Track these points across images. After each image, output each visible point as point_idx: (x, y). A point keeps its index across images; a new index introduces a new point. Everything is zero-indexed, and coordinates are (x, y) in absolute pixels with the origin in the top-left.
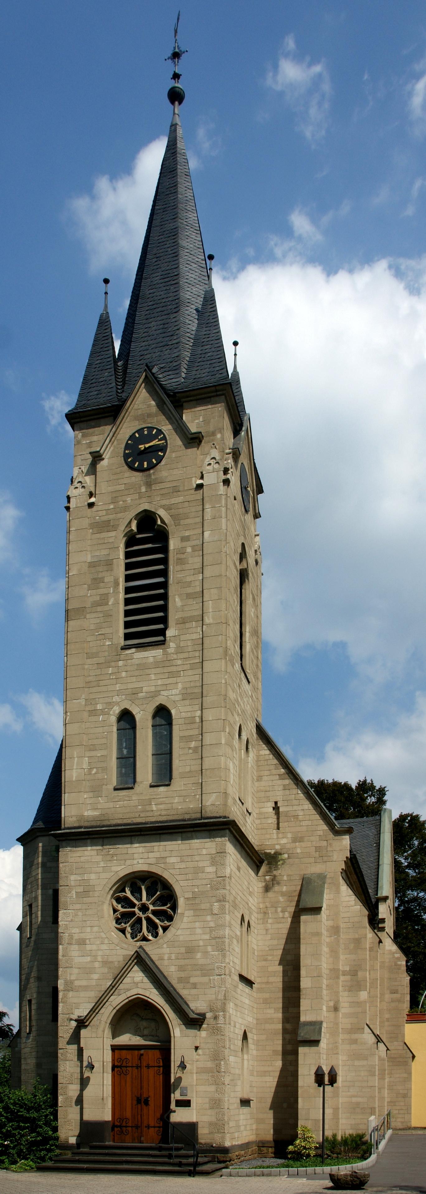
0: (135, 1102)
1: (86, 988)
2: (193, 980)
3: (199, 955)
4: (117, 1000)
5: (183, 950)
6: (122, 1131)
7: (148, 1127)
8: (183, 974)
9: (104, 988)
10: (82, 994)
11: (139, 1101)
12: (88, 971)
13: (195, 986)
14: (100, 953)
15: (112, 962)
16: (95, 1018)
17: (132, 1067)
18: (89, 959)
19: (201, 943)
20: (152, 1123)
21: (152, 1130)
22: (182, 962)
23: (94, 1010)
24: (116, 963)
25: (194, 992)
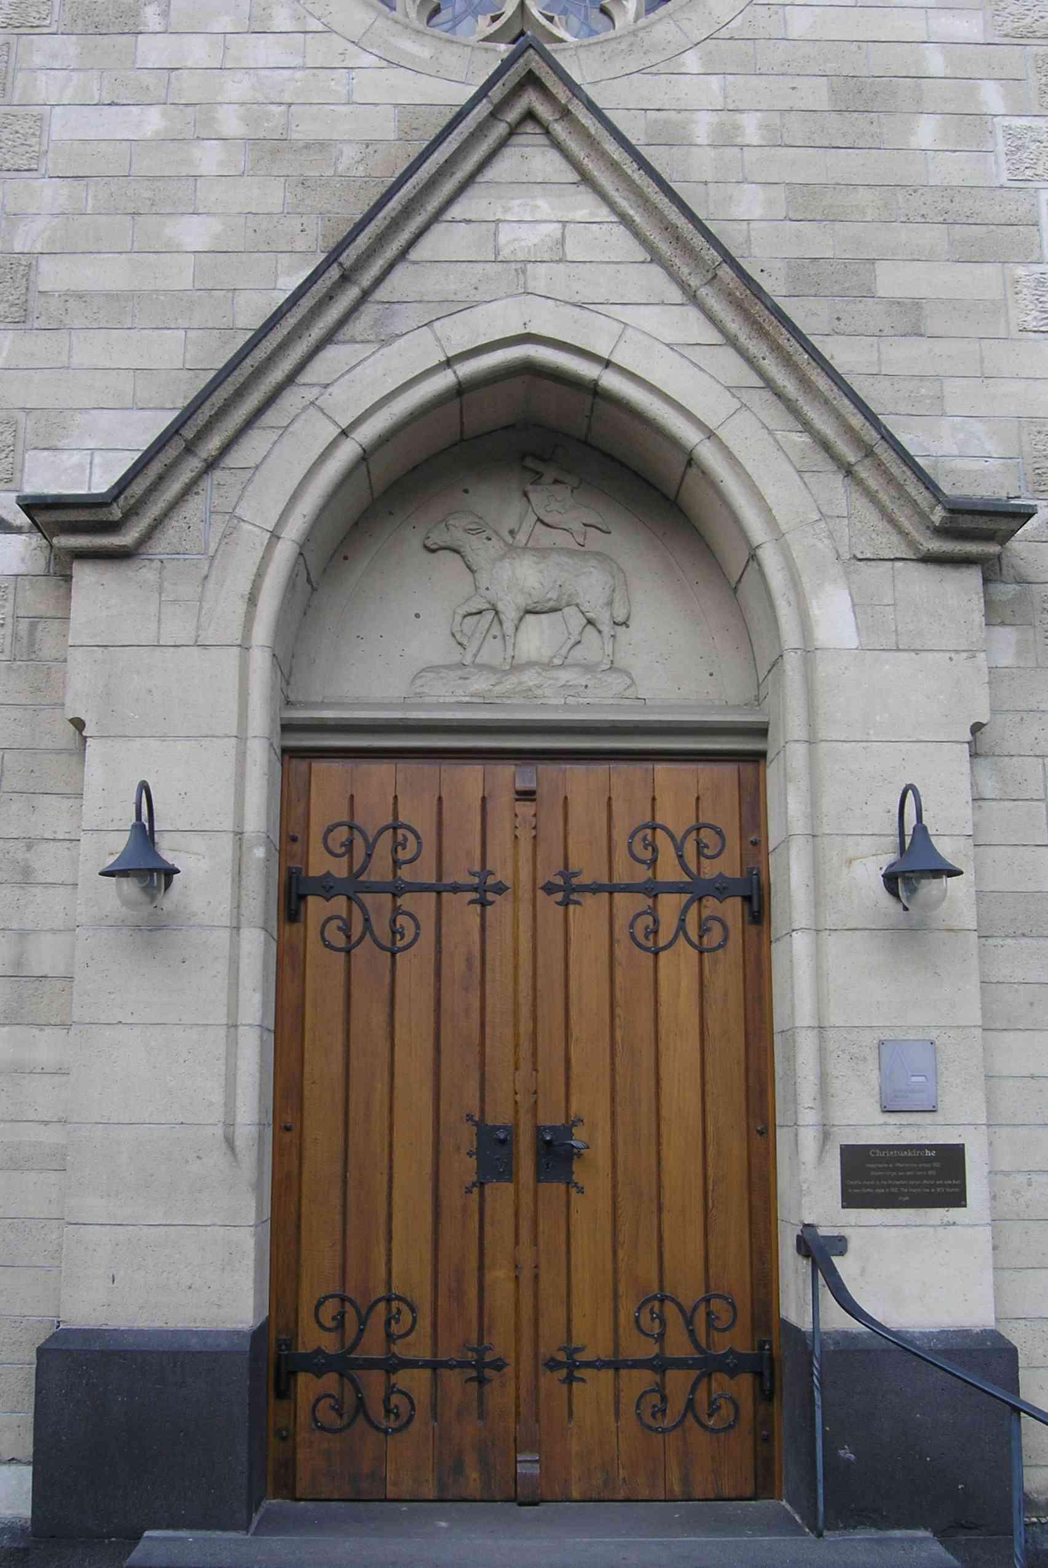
0: (463, 1167)
1: (118, 308)
2: (892, 281)
3: (926, 132)
4: (375, 378)
5: (815, 94)
6: (361, 1405)
7: (570, 1366)
8: (820, 242)
9: (252, 311)
10: (90, 349)
11: (494, 1152)
12: (140, 195)
13: (911, 319)
14: (236, 88)
15: (322, 145)
16: (194, 507)
17: (612, 889)
18: (153, 121)
19: (935, 62)
20: (594, 1340)
21: (595, 1388)
22: (812, 167)
23: (200, 434)
24: (350, 153)
25: (902, 355)
